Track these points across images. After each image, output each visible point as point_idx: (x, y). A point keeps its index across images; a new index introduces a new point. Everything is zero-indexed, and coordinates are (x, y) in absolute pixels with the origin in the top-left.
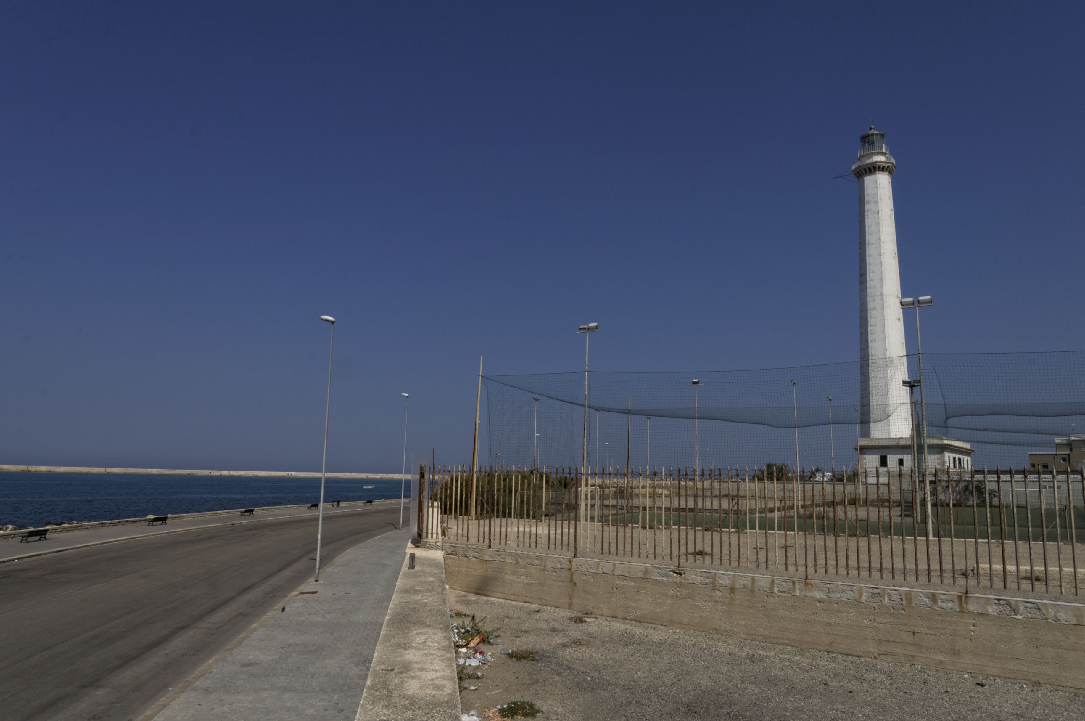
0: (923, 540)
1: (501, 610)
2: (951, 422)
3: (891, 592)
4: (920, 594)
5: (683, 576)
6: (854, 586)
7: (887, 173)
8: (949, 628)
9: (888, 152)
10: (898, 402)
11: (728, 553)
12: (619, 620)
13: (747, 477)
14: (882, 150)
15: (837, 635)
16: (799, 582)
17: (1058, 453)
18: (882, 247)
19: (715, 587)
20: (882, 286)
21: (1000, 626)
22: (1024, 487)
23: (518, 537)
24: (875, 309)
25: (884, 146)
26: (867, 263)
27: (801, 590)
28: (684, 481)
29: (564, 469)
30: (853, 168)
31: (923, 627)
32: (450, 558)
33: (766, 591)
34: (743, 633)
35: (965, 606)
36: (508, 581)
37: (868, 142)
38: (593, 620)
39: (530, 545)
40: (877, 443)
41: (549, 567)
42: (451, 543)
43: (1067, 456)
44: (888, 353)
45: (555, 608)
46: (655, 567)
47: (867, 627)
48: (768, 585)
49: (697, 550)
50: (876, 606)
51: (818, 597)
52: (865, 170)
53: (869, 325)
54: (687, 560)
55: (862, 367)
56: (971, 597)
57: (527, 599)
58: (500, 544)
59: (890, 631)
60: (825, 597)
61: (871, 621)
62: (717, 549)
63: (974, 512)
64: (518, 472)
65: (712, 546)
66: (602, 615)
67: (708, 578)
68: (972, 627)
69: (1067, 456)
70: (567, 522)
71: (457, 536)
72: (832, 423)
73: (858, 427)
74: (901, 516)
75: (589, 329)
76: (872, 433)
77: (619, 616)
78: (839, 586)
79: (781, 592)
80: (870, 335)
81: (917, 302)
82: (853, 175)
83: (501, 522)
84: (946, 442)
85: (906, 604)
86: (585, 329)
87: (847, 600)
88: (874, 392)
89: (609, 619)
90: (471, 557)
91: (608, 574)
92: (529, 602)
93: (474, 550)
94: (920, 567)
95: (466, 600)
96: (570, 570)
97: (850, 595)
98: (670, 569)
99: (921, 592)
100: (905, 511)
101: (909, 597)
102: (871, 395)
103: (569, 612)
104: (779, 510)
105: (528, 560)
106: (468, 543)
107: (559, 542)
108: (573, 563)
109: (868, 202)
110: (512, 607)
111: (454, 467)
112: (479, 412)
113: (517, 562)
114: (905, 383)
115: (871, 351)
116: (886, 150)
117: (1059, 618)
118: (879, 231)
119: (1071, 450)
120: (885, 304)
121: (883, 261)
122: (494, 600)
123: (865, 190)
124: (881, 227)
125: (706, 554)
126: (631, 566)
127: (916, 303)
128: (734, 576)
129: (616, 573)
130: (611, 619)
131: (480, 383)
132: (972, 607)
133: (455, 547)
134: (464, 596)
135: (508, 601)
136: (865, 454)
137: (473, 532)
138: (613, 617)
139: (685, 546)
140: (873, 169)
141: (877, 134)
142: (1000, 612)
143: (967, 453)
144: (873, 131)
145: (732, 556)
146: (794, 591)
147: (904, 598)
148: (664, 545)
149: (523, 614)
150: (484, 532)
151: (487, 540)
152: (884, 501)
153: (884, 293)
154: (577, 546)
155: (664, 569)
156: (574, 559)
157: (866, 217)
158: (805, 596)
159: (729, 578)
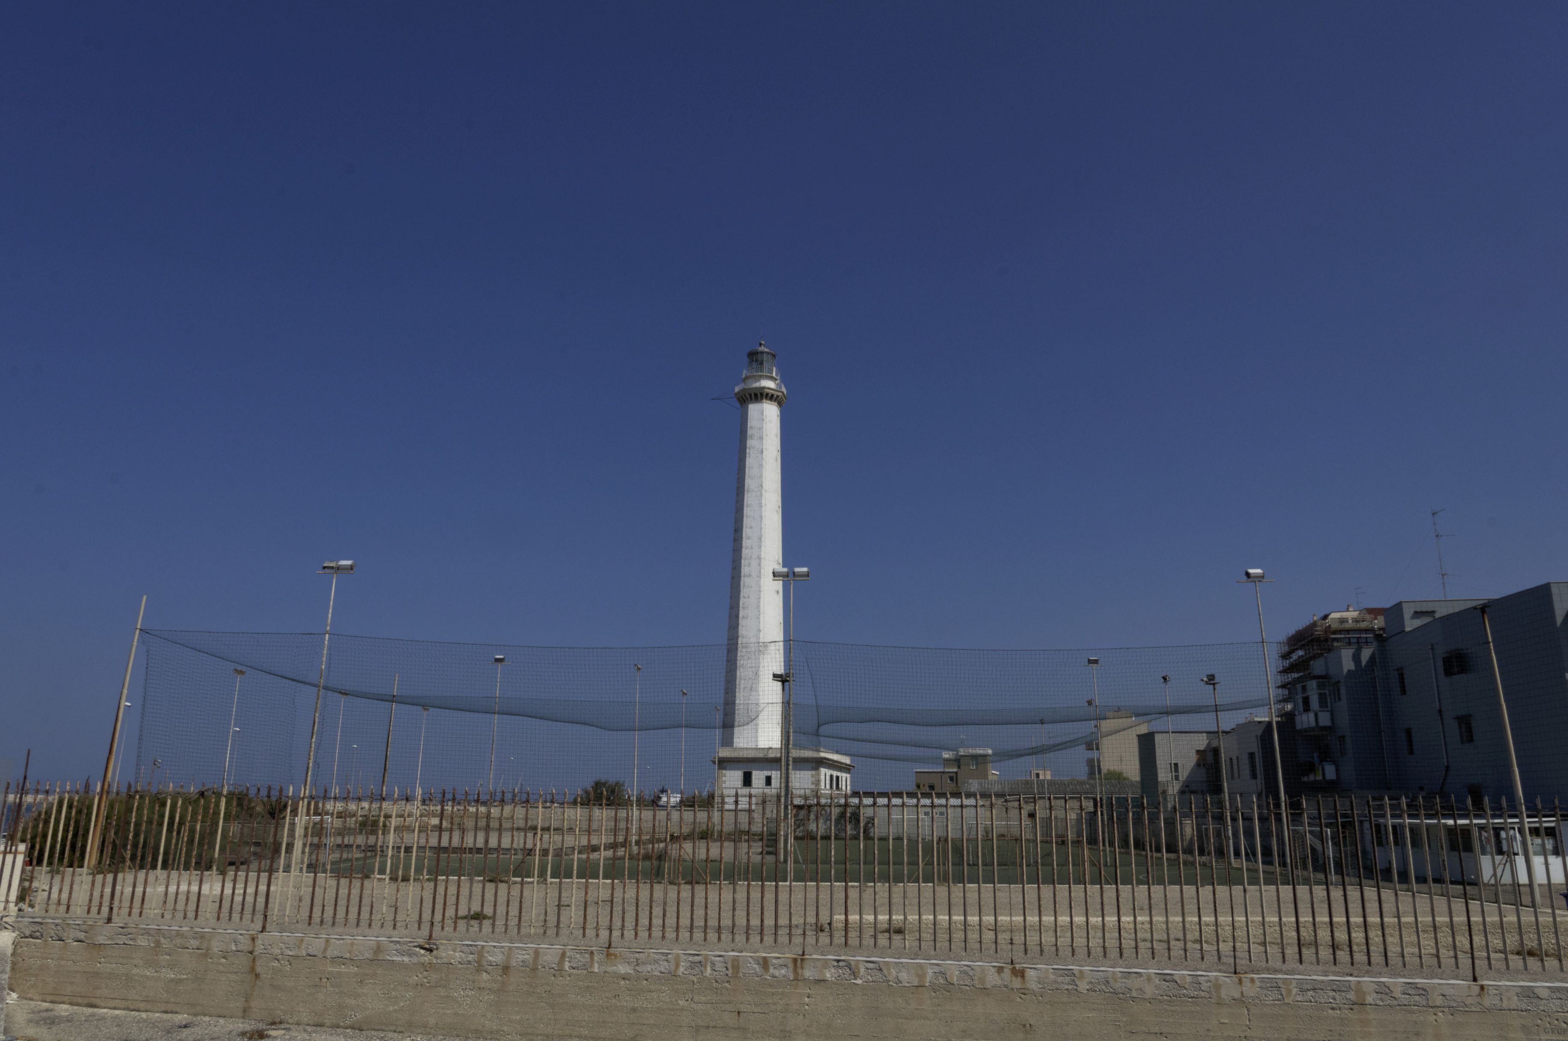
0: (1033, 887)
1: (115, 1029)
2: (823, 729)
3: (715, 958)
4: (750, 959)
5: (435, 952)
6: (670, 953)
7: (776, 404)
8: (781, 1002)
9: (778, 378)
10: (766, 701)
11: (517, 914)
12: (328, 1029)
13: (540, 804)
14: (772, 373)
15: (644, 1025)
16: (600, 952)
17: (947, 770)
18: (764, 497)
19: (481, 968)
20: (760, 547)
21: (838, 995)
23: (165, 902)
24: (749, 576)
25: (774, 369)
26: (745, 515)
27: (600, 964)
28: (473, 806)
29: (259, 789)
30: (737, 390)
31: (751, 1004)
32: (28, 944)
33: (553, 968)
34: (516, 1033)
35: (800, 971)
36: (136, 978)
37: (756, 361)
38: (283, 1032)
39: (185, 914)
40: (741, 754)
41: (216, 950)
42: (33, 918)
43: (954, 775)
44: (761, 635)
45: (217, 1019)
46: (392, 942)
47: (682, 1010)
48: (557, 960)
49: (472, 913)
50: (695, 980)
51: (623, 972)
52: (750, 395)
54: (455, 928)
55: (729, 651)
56: (807, 959)
57: (170, 1007)
58: (130, 915)
59: (711, 1012)
60: (632, 972)
61: (687, 1000)
62: (501, 909)
63: (817, 849)
64: (179, 793)
65: (495, 906)
66: (298, 1024)
67: (471, 954)
68: (806, 999)
69: (954, 775)
70: (267, 874)
71: (48, 904)
73: (718, 732)
74: (761, 853)
75: (338, 568)
77: (328, 1022)
78: (651, 955)
79: (574, 968)
80: (741, 609)
82: (735, 399)
83: (135, 878)
84: (823, 755)
85: (733, 974)
86: (332, 568)
87: (659, 974)
88: (742, 686)
89: (309, 1029)
90: (70, 941)
91: (315, 956)
92: (172, 1012)
93: (77, 927)
94: (766, 922)
95: (49, 1018)
96: (251, 953)
97: (664, 966)
98: (416, 944)
99: (751, 957)
100: (767, 846)
101: (736, 965)
102: (737, 690)
103: (243, 1023)
104: (608, 847)
105: (178, 941)
106: (67, 916)
107: (237, 908)
108: (259, 942)
109: (751, 436)
110: (138, 1022)
111: (58, 783)
112: (128, 690)
113: (158, 944)
114: (776, 676)
115: (742, 631)
116: (777, 375)
117: (900, 979)
118: (761, 476)
119: (959, 767)
120: (762, 571)
121: (763, 515)
122: (107, 1013)
124: (764, 471)
125: (485, 917)
126: (355, 942)
127: (791, 575)
128: (510, 948)
129: (329, 954)
130: (314, 1028)
131: (136, 640)
132: (808, 973)
133: (41, 923)
134: (47, 1010)
135: (133, 1013)
136: (725, 769)
137: (81, 895)
138: (317, 1025)
139: (455, 906)
140: (760, 396)
141: (767, 353)
142: (839, 976)
143: (847, 769)
144: (762, 349)
145: (523, 919)
146: (592, 966)
147: (729, 966)
148: (409, 907)
149: (158, 1032)
150: (102, 896)
151: (105, 910)
152: (742, 832)
153: (762, 556)
154: (269, 914)
155: (406, 943)
156: (260, 936)
157: (747, 455)
158: (606, 972)
159: (503, 952)
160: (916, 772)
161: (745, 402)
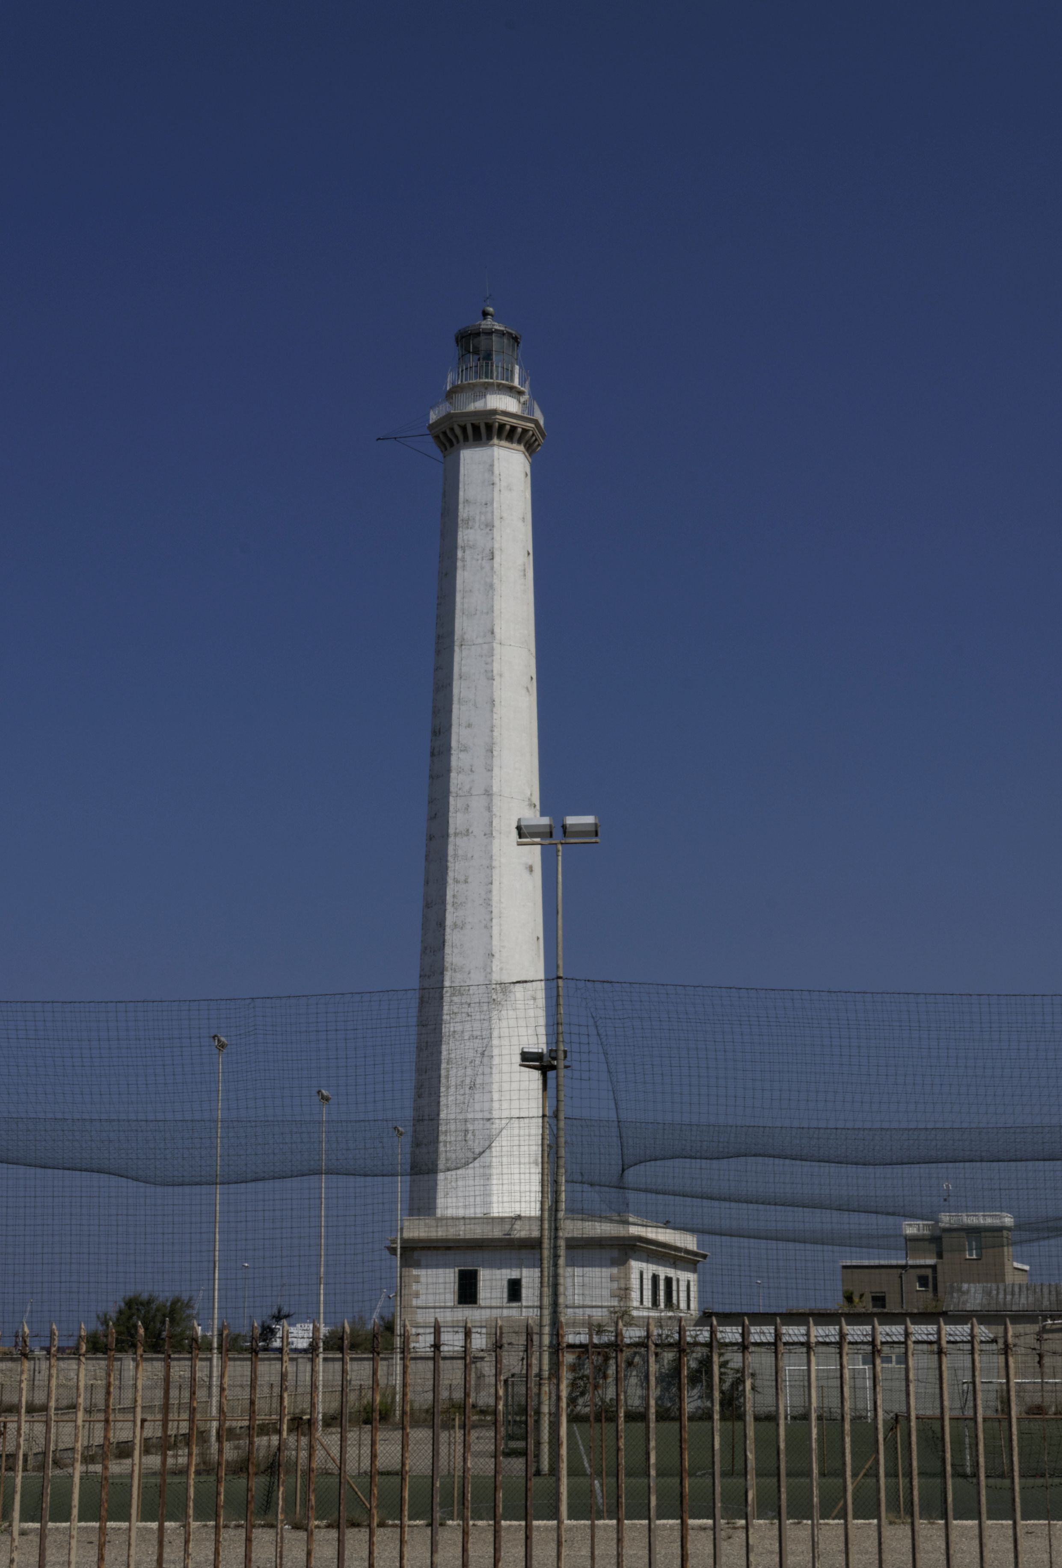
7: (522, 447)
9: (525, 389)
14: (512, 380)
17: (910, 1262)
18: (496, 658)
22: (805, 1361)
24: (467, 833)
25: (517, 368)
30: (433, 417)
37: (476, 352)
40: (464, 1232)
43: (929, 1272)
52: (464, 429)
53: (450, 880)
69: (929, 1272)
72: (329, 1172)
76: (440, 1201)
80: (449, 908)
81: (561, 830)
82: (430, 439)
100: (510, 1437)
109: (467, 521)
114: (528, 1058)
115: (452, 956)
116: (522, 383)
118: (491, 610)
119: (940, 1255)
120: (495, 822)
123: (461, 485)
124: (496, 598)
127: (557, 832)
136: (418, 1265)
141: (502, 334)
144: (489, 323)
153: (495, 789)
157: (459, 564)
160: (845, 1267)
161: (452, 445)
